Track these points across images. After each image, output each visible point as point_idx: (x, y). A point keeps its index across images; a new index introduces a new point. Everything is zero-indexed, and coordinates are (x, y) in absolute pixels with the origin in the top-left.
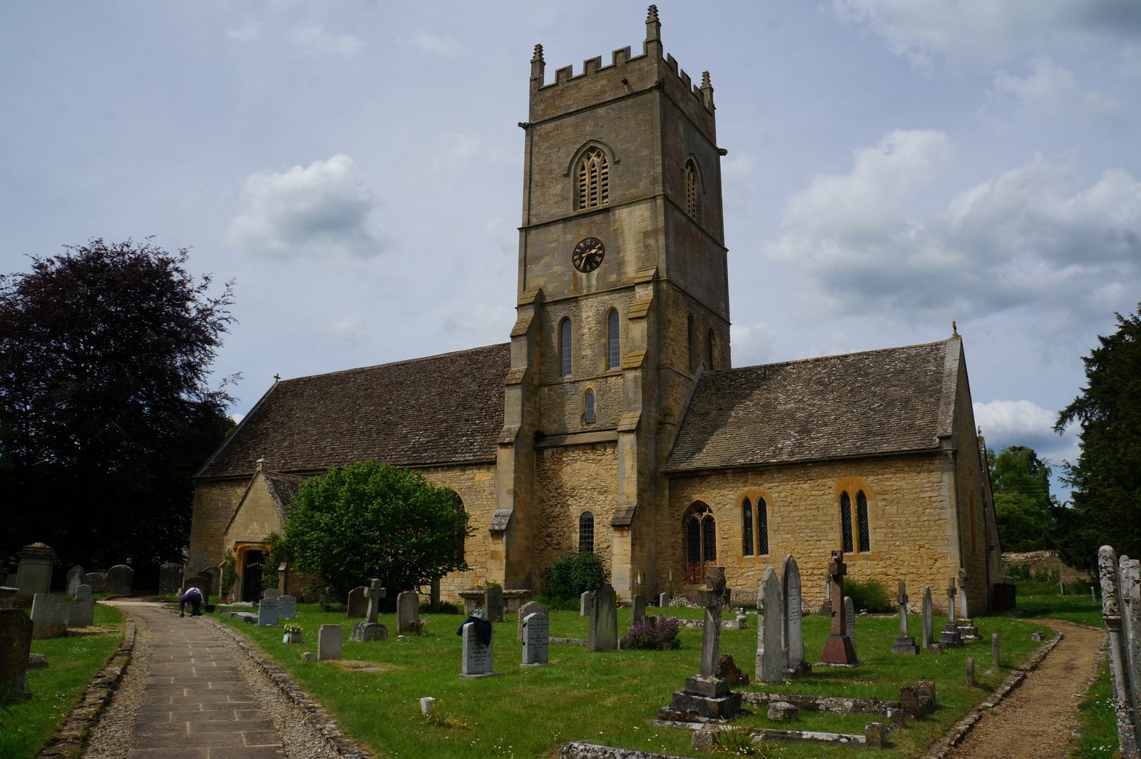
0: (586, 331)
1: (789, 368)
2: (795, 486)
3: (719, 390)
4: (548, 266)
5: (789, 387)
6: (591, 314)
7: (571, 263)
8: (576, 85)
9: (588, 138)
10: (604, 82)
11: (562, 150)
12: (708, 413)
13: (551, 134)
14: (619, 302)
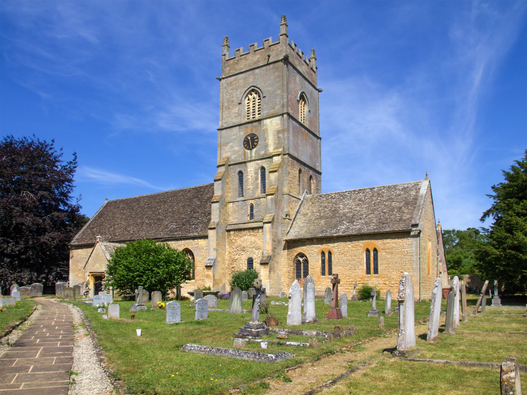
0: (249, 177)
3: (313, 203)
4: (232, 147)
7: (243, 146)
8: (245, 58)
9: (251, 85)
10: (259, 56)
11: (238, 91)
12: (307, 214)
14: (264, 163)
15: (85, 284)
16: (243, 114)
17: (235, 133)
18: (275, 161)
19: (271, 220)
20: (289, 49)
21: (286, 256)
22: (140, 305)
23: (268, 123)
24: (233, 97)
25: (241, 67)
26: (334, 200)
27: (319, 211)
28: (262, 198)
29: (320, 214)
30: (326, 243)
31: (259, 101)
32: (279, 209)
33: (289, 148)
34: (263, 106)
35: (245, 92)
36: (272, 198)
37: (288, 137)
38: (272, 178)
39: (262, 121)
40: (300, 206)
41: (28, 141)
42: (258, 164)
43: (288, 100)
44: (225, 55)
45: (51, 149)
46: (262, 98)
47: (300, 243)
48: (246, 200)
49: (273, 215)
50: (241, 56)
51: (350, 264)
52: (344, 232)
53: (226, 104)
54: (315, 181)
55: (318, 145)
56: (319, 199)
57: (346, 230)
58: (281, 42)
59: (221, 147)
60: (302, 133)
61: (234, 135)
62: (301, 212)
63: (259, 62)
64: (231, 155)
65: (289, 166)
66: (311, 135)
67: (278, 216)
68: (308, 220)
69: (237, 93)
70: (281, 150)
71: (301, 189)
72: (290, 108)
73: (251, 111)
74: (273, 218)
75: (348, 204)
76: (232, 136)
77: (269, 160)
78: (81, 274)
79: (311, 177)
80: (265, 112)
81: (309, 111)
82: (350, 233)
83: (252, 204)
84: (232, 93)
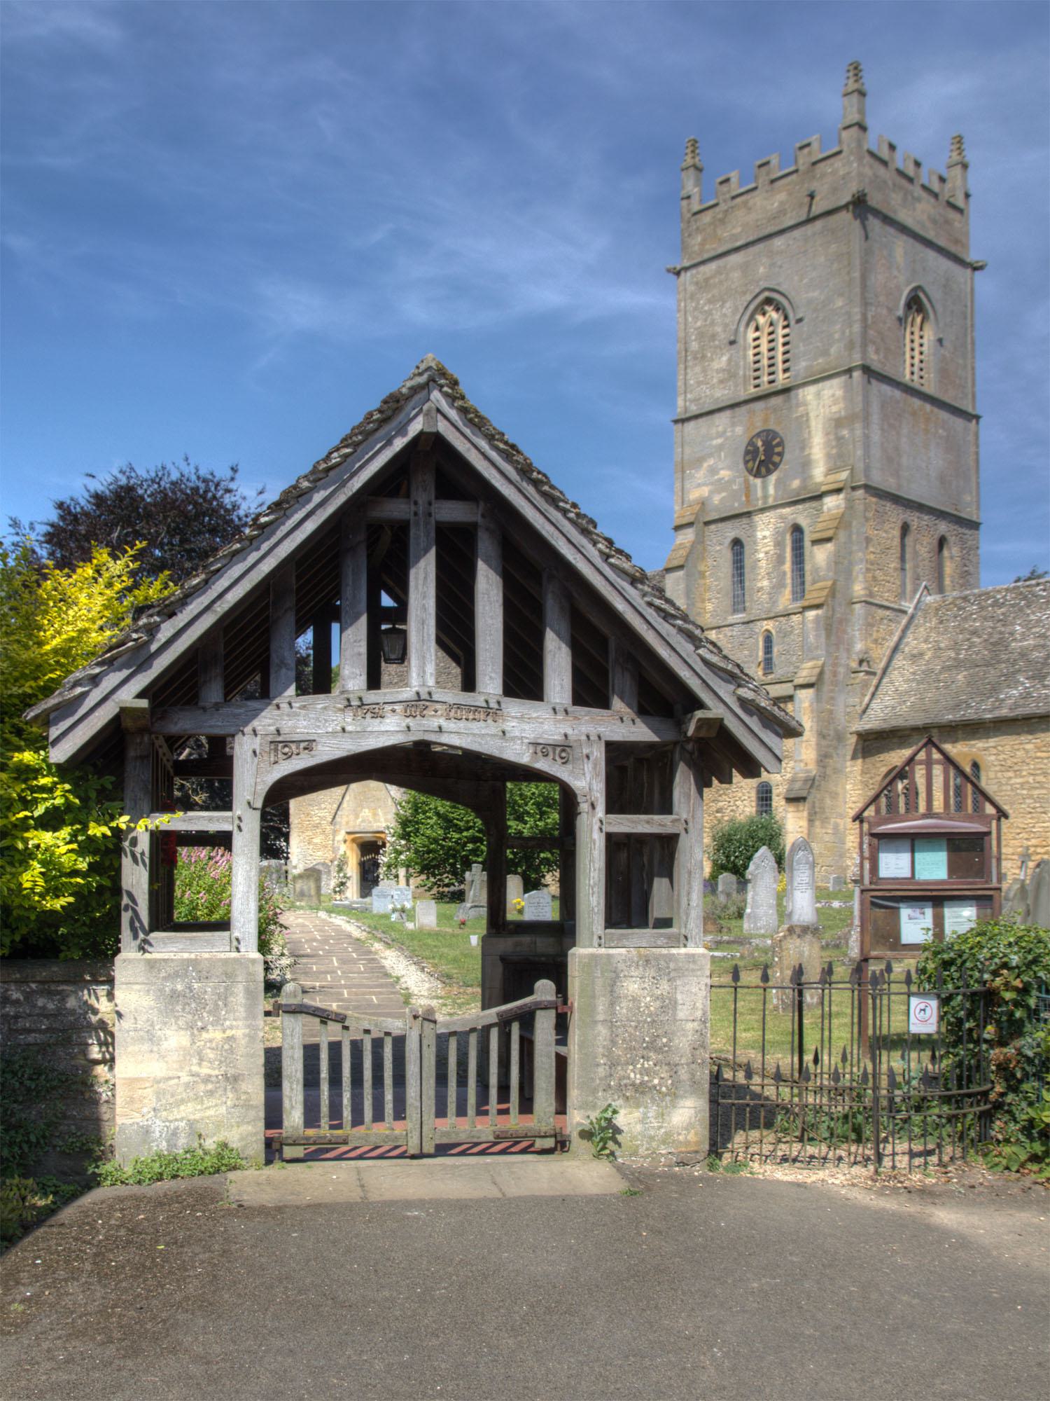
0: (761, 555)
1: (1038, 588)
2: (1016, 747)
3: (941, 622)
4: (713, 471)
5: (1032, 617)
6: (767, 533)
7: (742, 466)
8: (745, 203)
9: (763, 284)
10: (782, 196)
11: (728, 305)
12: (921, 654)
13: (712, 281)
14: (800, 515)
15: (336, 863)
16: (741, 373)
17: (720, 429)
18: (829, 510)
19: (813, 680)
20: (871, 167)
21: (859, 778)
22: (476, 906)
23: (809, 397)
24: (713, 323)
25: (735, 231)
26: (999, 612)
27: (955, 646)
28: (795, 614)
29: (958, 654)
30: (964, 739)
31: (786, 331)
32: (837, 645)
33: (867, 469)
34: (799, 348)
35: (747, 307)
36: (817, 616)
37: (867, 437)
38: (820, 556)
39: (793, 393)
40: (904, 631)
41: (169, 474)
42: (782, 517)
43: (865, 327)
44: (689, 197)
45: (228, 491)
46: (792, 323)
47: (895, 740)
48: (752, 621)
49: (820, 663)
50: (734, 198)
51: (1031, 797)
52: (1016, 705)
53: (694, 346)
54: (955, 551)
55: (971, 438)
56: (960, 609)
57: (1022, 702)
58: (845, 149)
59: (683, 472)
60: (914, 414)
61: (719, 435)
62: (907, 649)
63: (785, 214)
64: (711, 492)
65: (867, 519)
66: (944, 415)
67: (835, 665)
68: (923, 672)
69: (724, 310)
70: (844, 475)
71: (908, 581)
72: (871, 349)
73: (765, 362)
74: (821, 674)
75: (1039, 621)
76: (712, 439)
77: (814, 504)
78: (322, 837)
79: (942, 542)
80: (802, 365)
81: (940, 341)
82: (1031, 708)
83: (767, 631)
84: (709, 313)
